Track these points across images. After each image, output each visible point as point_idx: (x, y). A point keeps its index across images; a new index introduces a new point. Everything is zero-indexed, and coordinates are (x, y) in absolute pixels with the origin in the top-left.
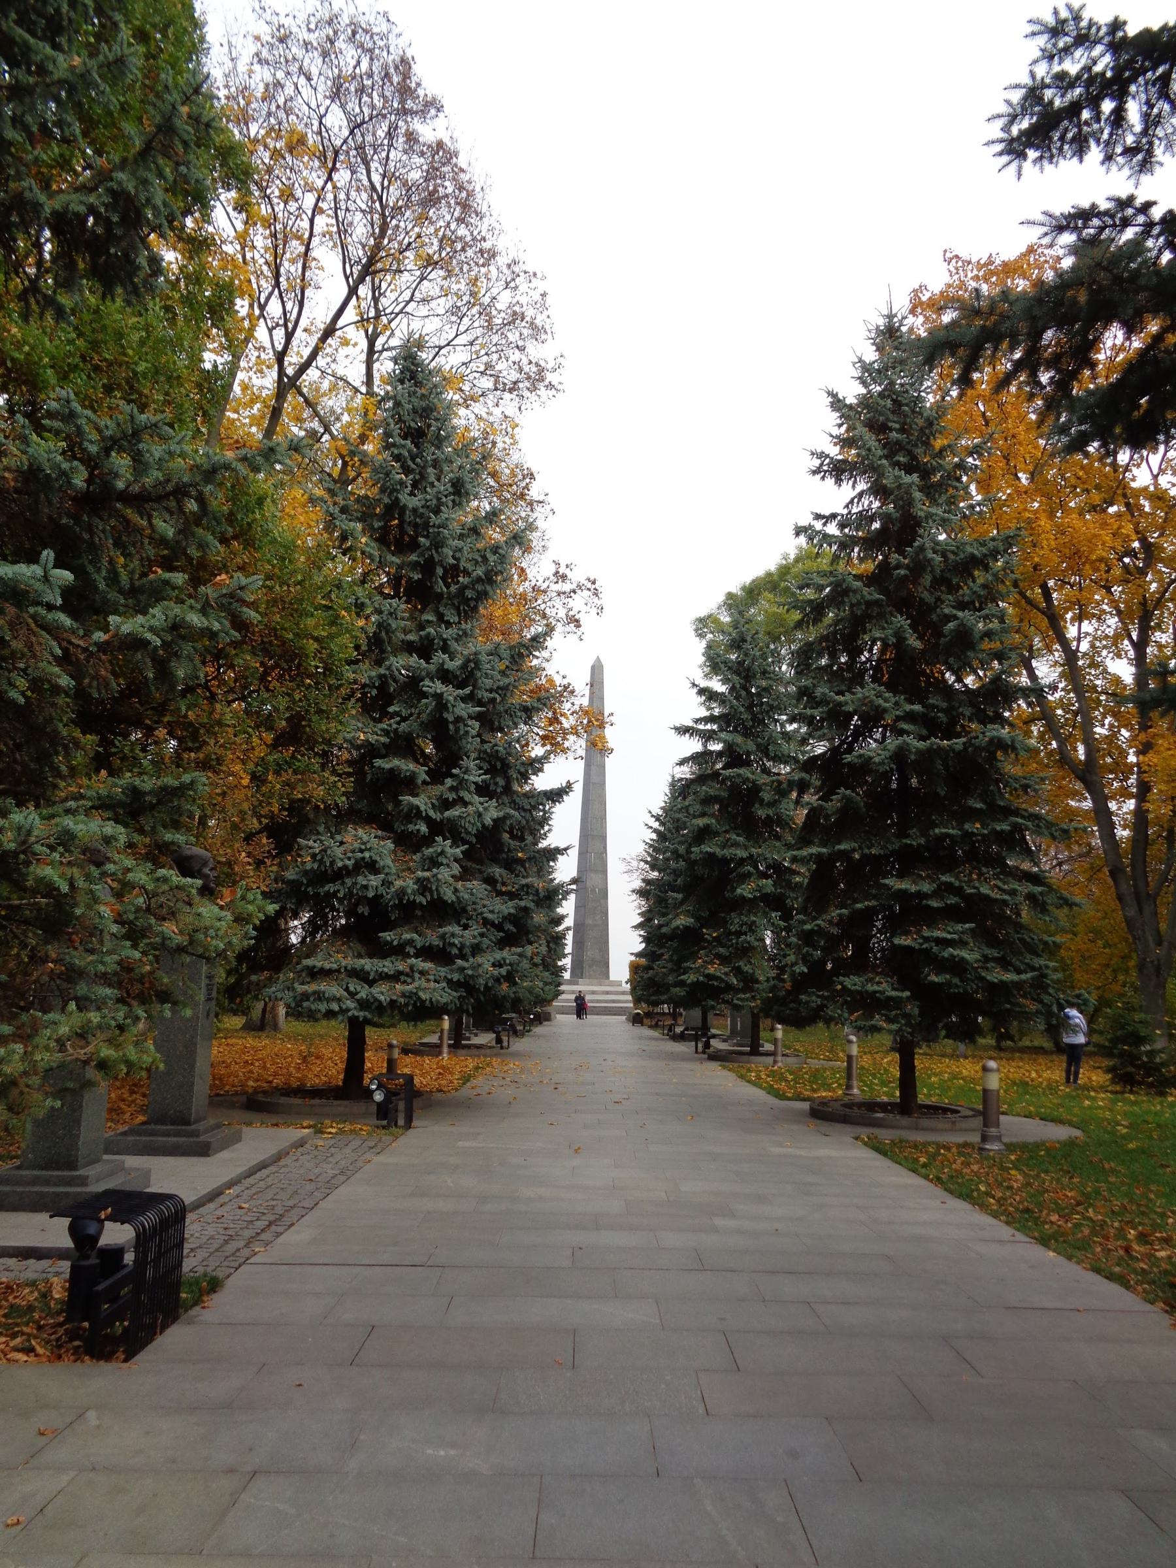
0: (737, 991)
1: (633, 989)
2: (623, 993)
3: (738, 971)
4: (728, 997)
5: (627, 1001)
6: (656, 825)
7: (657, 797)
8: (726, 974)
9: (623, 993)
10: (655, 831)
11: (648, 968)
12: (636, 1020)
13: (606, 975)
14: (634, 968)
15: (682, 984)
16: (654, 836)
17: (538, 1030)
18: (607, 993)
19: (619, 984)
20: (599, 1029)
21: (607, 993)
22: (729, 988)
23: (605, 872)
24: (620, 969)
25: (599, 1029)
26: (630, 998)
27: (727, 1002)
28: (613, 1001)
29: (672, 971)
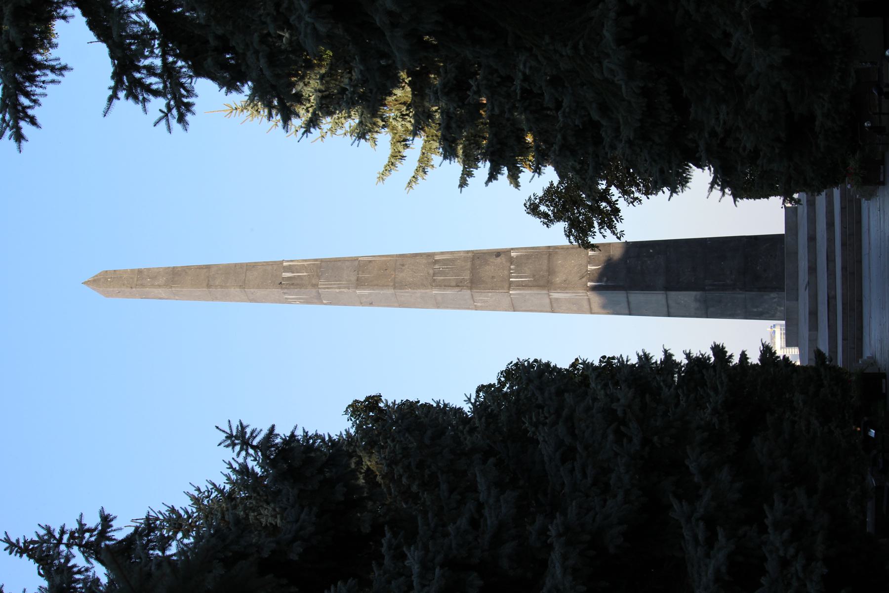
2: (811, 204)
9: (811, 204)
18: (812, 239)
21: (812, 239)
28: (830, 225)
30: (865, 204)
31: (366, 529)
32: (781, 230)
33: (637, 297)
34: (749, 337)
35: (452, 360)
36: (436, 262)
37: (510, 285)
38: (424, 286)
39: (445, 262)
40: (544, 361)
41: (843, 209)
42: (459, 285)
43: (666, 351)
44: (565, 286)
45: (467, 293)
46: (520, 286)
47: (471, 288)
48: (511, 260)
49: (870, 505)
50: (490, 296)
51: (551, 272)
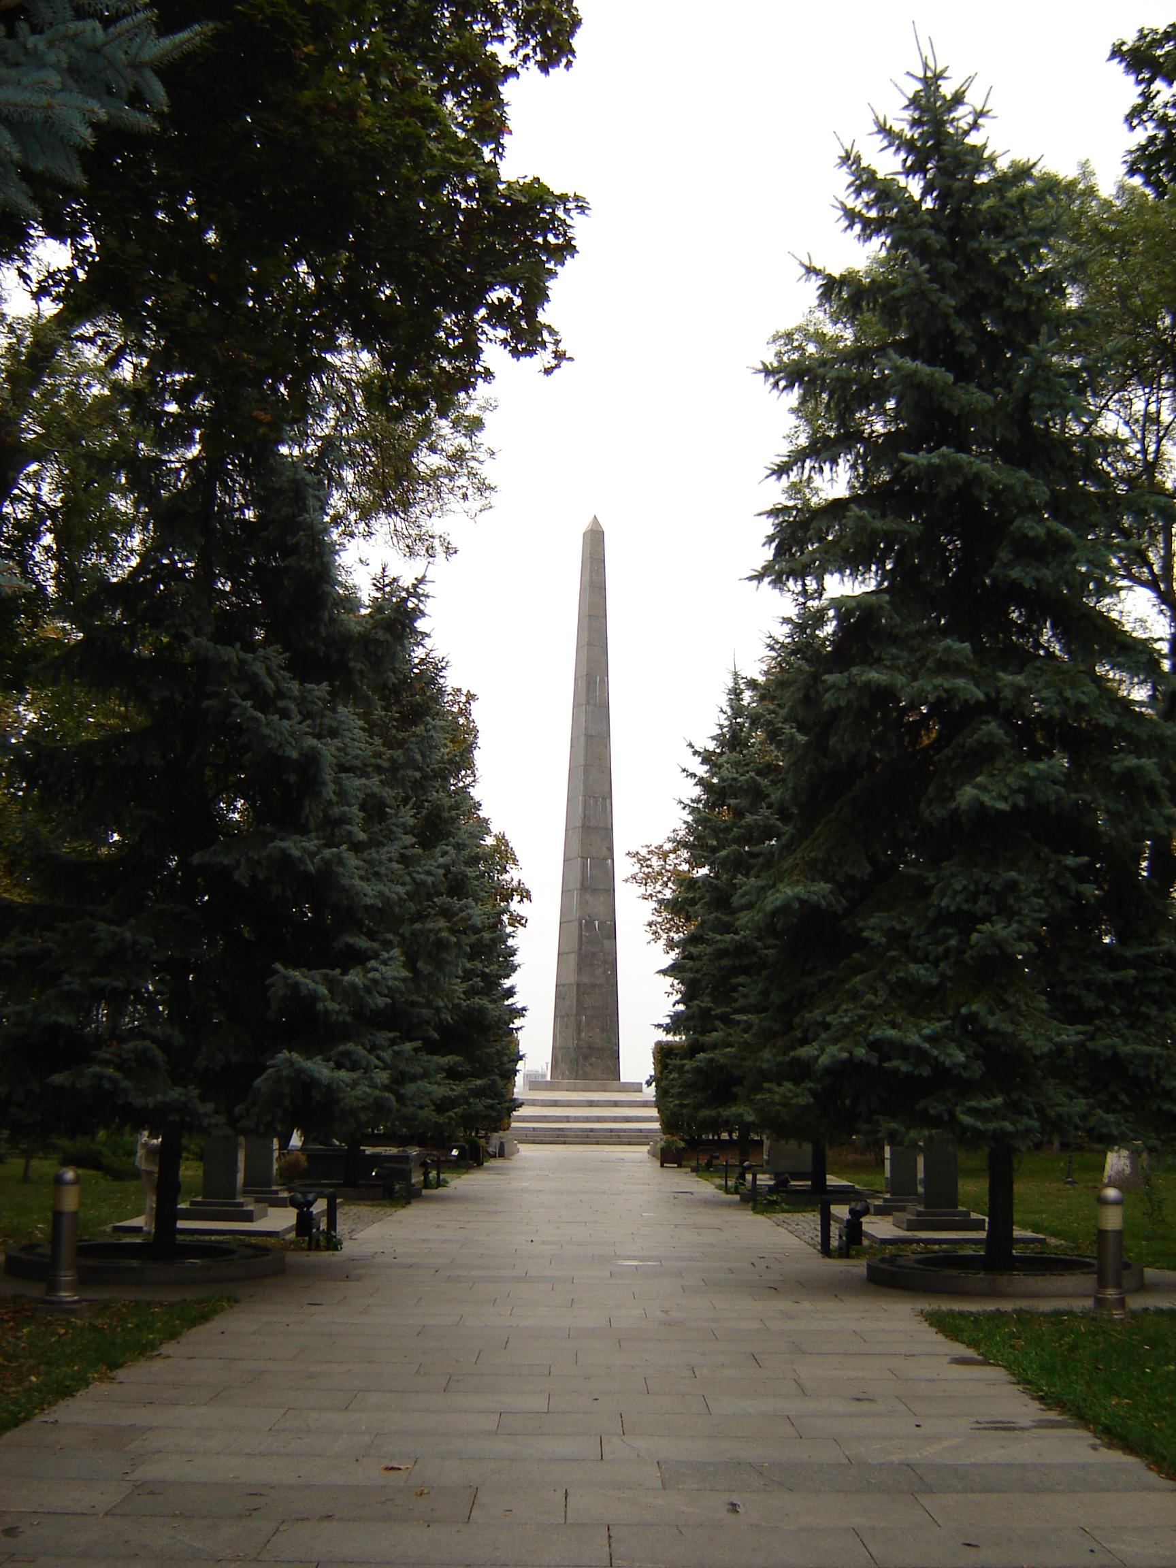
0: (965, 1088)
1: (662, 1093)
2: (645, 1104)
3: (969, 1030)
4: (936, 1108)
5: (650, 1119)
6: (702, 770)
7: (706, 722)
8: (932, 1039)
9: (645, 1104)
10: (701, 782)
11: (693, 1049)
12: (668, 1157)
13: (615, 1073)
14: (663, 1054)
15: (800, 1071)
16: (697, 791)
17: (461, 1183)
18: (616, 1104)
19: (637, 1088)
20: (583, 1209)
21: (616, 1104)
22: (943, 1077)
23: (611, 891)
24: (637, 1062)
25: (583, 1209)
26: (654, 1112)
27: (936, 1122)
28: (628, 1119)
29: (767, 1036)
30: (646, 1148)
31: (949, 1051)
32: (624, 1078)
33: (572, 959)
34: (536, 1041)
35: (516, 793)
36: (604, 799)
37: (584, 858)
38: (585, 789)
39: (604, 807)
40: (575, 42)
41: (641, 1130)
42: (585, 817)
43: (524, 1009)
44: (583, 903)
45: (579, 823)
46: (584, 866)
47: (583, 827)
48: (605, 859)
49: (393, 1151)
50: (576, 843)
51: (594, 891)
